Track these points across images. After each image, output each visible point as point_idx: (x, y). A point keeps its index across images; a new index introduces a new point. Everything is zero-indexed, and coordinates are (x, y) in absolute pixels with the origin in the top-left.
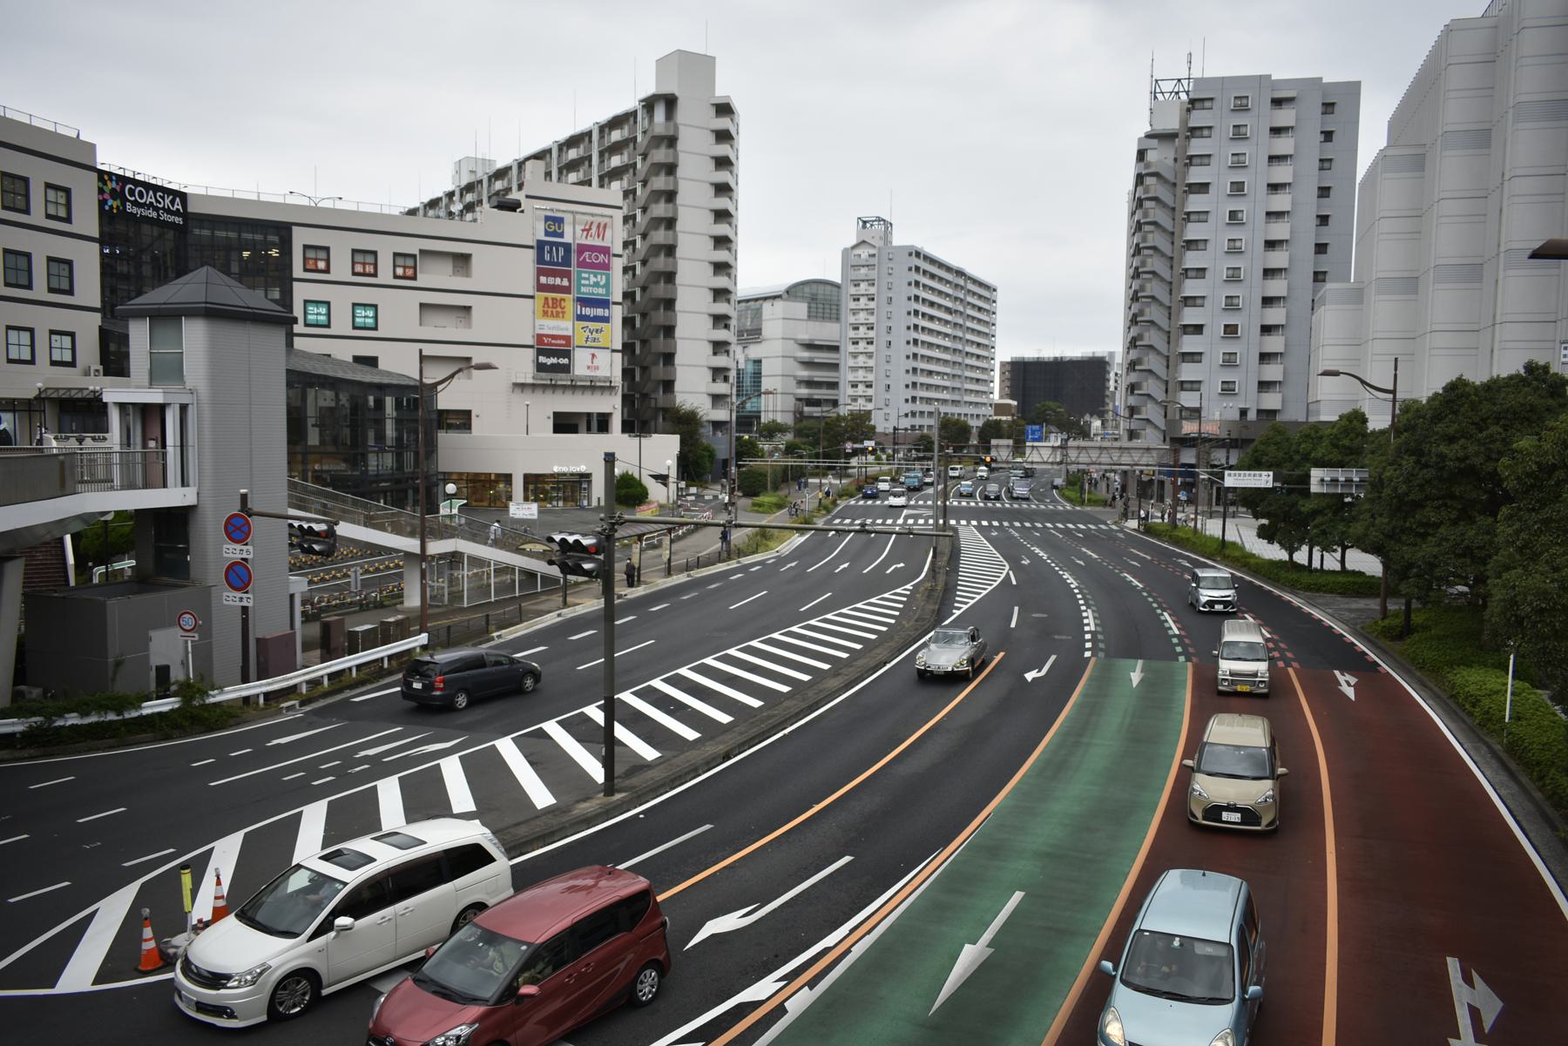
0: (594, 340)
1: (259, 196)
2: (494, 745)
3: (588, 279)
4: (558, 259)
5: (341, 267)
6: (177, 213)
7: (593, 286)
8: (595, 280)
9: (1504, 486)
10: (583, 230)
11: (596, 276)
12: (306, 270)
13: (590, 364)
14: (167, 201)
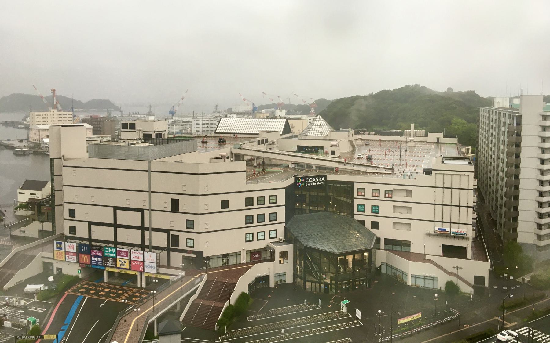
0: (123, 265)
3: (108, 250)
4: (85, 250)
5: (368, 195)
7: (110, 253)
8: (111, 250)
10: (68, 247)
11: (111, 249)
12: (358, 195)
14: (319, 179)
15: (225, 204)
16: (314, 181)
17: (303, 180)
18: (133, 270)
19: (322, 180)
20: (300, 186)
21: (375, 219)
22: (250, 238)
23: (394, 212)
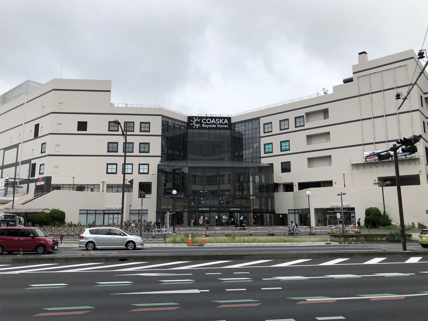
1: (211, 116)
2: (32, 164)
6: (226, 124)
9: (191, 239)
13: (342, 193)
15: (82, 126)
16: (213, 123)
17: (199, 121)
18: (230, 259)
19: (225, 122)
20: (191, 124)
21: (285, 159)
22: (112, 169)
23: (308, 144)
